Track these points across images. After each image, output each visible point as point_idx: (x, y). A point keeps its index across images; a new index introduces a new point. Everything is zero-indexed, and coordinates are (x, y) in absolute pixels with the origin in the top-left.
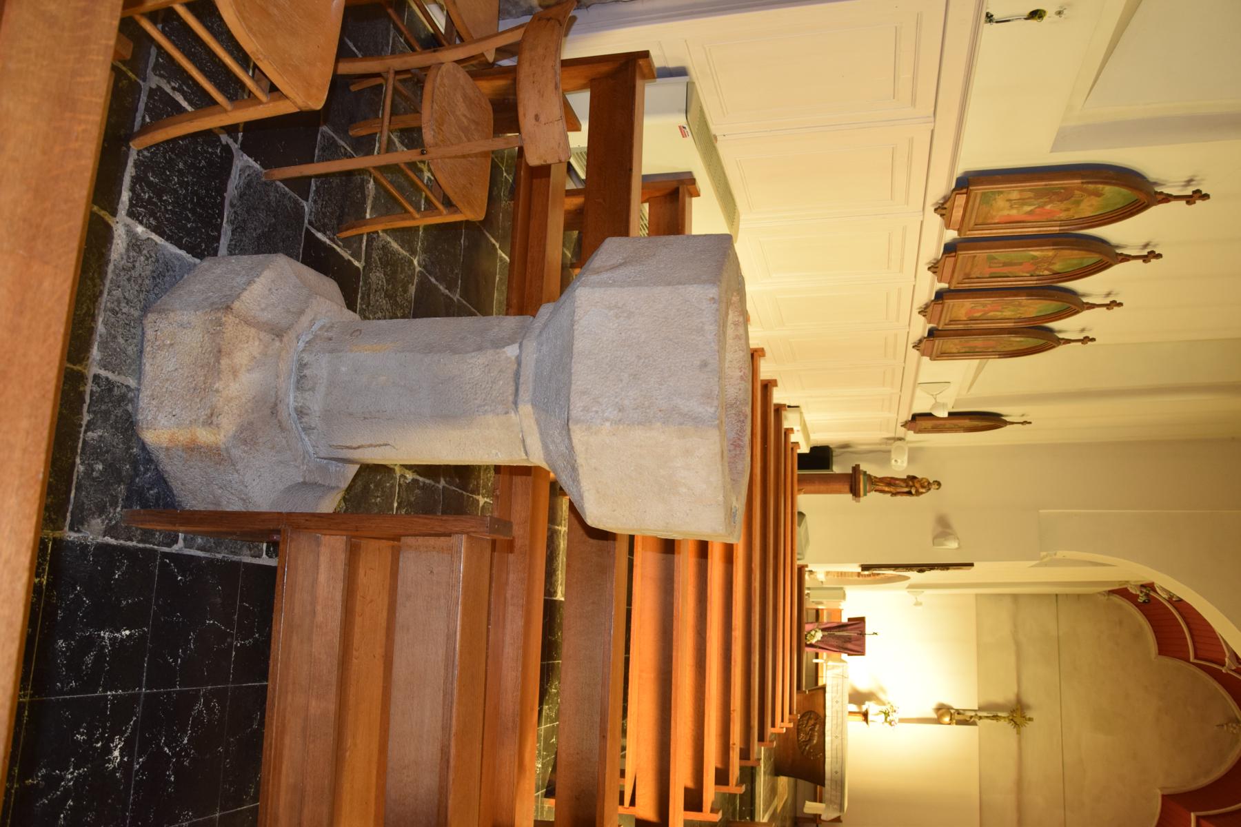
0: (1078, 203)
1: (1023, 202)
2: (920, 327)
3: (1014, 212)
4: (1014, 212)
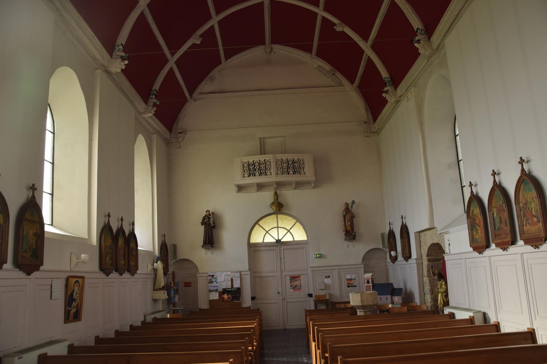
2: (126, 275)
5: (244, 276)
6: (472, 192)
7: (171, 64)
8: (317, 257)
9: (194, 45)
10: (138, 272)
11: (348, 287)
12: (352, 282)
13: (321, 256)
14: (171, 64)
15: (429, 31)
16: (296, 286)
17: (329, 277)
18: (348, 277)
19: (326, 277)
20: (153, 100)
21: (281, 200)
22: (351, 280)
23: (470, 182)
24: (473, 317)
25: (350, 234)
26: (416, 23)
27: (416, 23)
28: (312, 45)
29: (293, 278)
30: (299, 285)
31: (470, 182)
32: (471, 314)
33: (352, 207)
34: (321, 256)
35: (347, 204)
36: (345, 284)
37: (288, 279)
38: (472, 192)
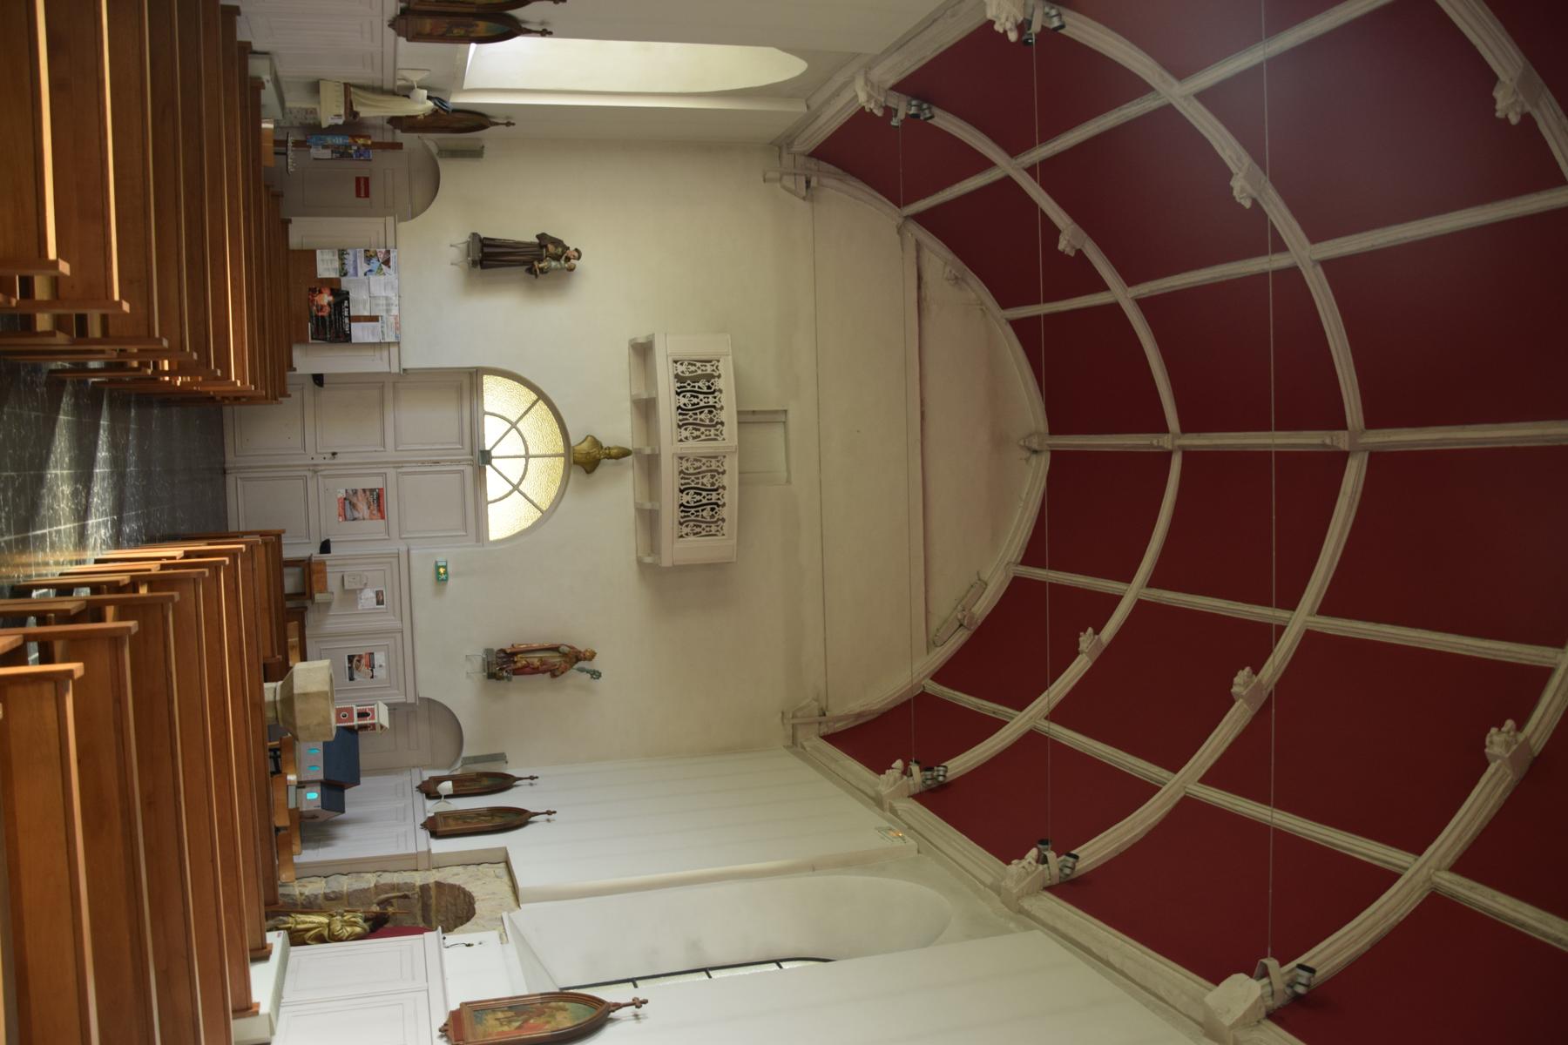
0: (552, 1016)
1: (510, 1021)
3: (506, 1028)
4: (506, 1028)
5: (385, 353)
6: (618, 1006)
7: (1005, 166)
8: (438, 568)
9: (1053, 232)
10: (402, 40)
11: (351, 658)
12: (363, 668)
13: (441, 579)
14: (1005, 166)
15: (1071, 890)
16: (353, 506)
17: (380, 602)
18: (379, 659)
19: (379, 594)
20: (904, 108)
21: (606, 466)
22: (371, 666)
23: (645, 1002)
24: (257, 1013)
25: (505, 665)
26: (1094, 852)
27: (1094, 852)
28: (1268, 604)
29: (377, 499)
30: (356, 515)
31: (645, 1002)
32: (265, 1008)
33: (582, 670)
34: (441, 579)
35: (593, 655)
36: (359, 647)
37: (374, 483)
38: (618, 1006)
